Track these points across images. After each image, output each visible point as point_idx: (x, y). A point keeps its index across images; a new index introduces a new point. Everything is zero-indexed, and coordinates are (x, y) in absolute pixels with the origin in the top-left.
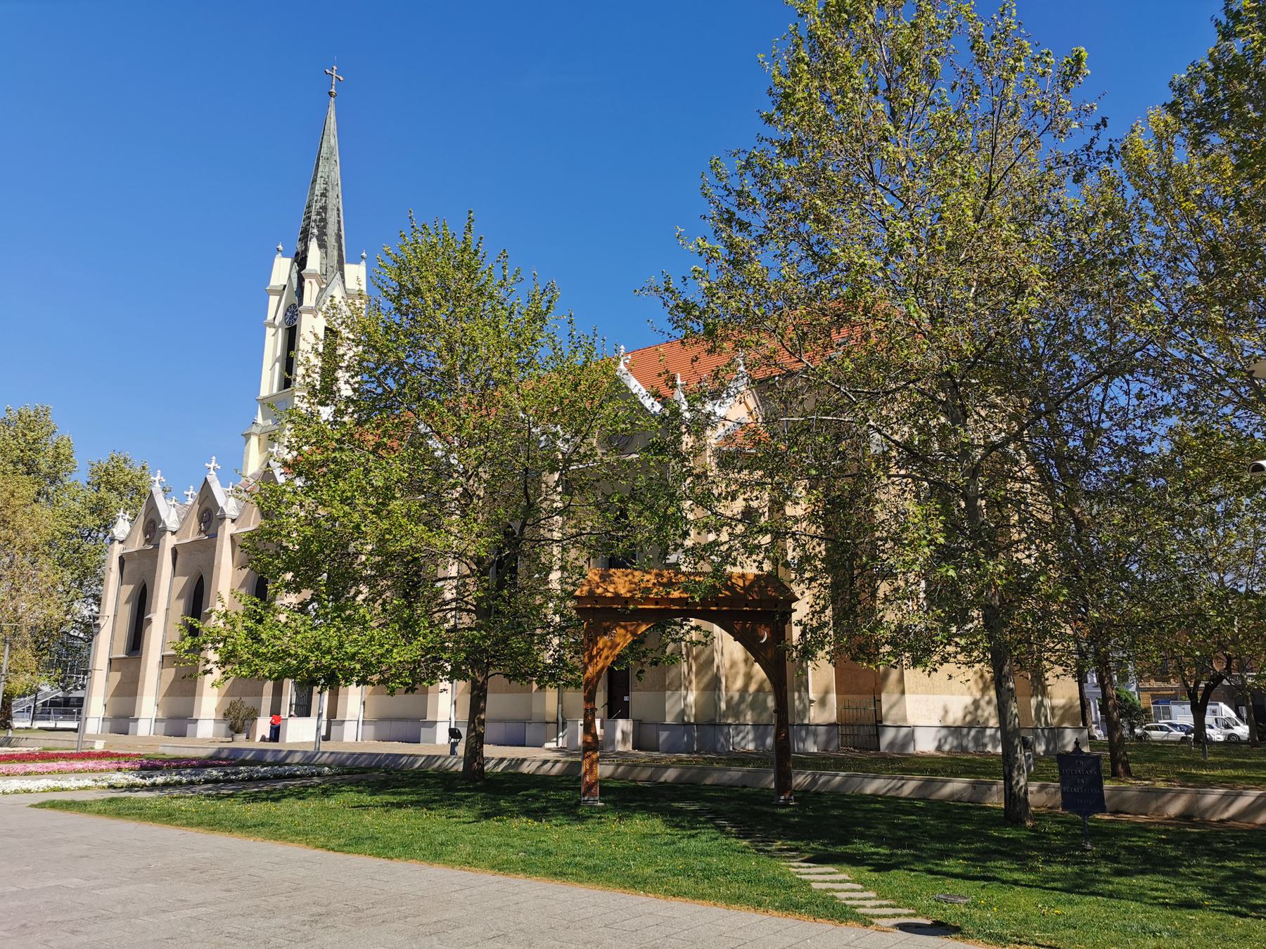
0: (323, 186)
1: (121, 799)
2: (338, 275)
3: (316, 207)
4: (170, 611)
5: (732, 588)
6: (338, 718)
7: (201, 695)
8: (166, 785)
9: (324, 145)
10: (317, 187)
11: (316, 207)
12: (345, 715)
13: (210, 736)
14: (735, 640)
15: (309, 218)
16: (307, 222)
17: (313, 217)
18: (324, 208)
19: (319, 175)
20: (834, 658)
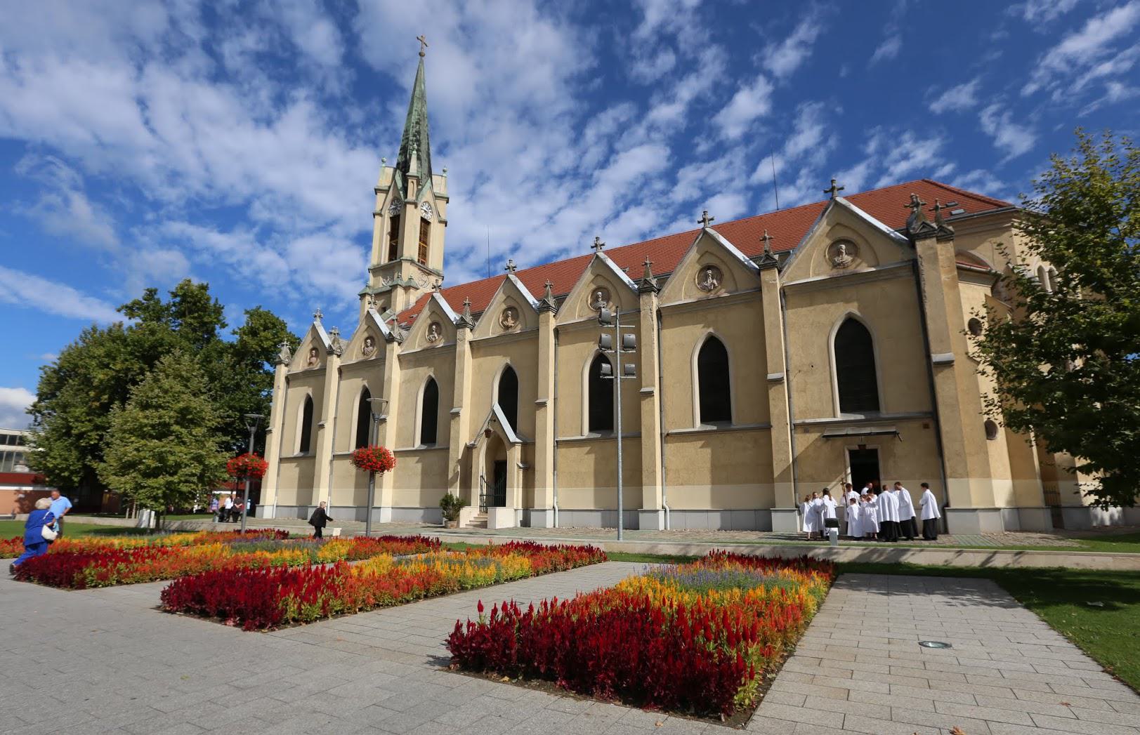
0: (417, 117)
1: (787, 544)
2: (429, 181)
3: (412, 131)
4: (338, 420)
5: (593, 73)
6: (261, 504)
7: (381, 487)
8: (671, 544)
9: (418, 89)
10: (413, 117)
11: (412, 131)
12: (265, 503)
13: (389, 521)
14: (772, 426)
15: (408, 138)
16: (405, 141)
17: (411, 138)
18: (418, 132)
19: (415, 108)
20: (573, 622)
